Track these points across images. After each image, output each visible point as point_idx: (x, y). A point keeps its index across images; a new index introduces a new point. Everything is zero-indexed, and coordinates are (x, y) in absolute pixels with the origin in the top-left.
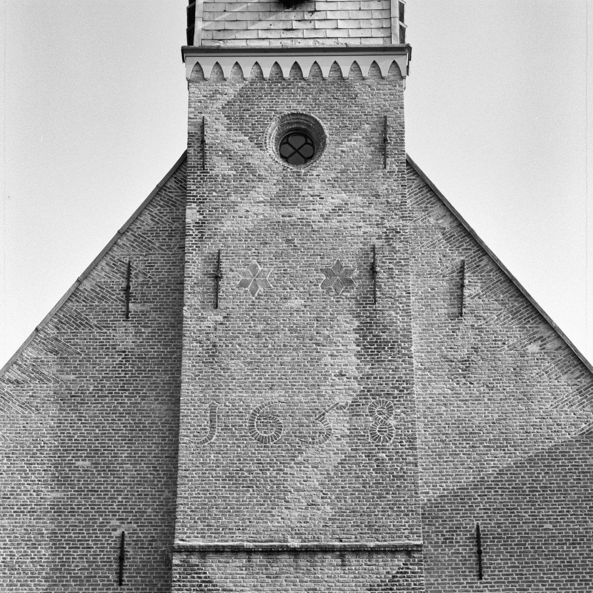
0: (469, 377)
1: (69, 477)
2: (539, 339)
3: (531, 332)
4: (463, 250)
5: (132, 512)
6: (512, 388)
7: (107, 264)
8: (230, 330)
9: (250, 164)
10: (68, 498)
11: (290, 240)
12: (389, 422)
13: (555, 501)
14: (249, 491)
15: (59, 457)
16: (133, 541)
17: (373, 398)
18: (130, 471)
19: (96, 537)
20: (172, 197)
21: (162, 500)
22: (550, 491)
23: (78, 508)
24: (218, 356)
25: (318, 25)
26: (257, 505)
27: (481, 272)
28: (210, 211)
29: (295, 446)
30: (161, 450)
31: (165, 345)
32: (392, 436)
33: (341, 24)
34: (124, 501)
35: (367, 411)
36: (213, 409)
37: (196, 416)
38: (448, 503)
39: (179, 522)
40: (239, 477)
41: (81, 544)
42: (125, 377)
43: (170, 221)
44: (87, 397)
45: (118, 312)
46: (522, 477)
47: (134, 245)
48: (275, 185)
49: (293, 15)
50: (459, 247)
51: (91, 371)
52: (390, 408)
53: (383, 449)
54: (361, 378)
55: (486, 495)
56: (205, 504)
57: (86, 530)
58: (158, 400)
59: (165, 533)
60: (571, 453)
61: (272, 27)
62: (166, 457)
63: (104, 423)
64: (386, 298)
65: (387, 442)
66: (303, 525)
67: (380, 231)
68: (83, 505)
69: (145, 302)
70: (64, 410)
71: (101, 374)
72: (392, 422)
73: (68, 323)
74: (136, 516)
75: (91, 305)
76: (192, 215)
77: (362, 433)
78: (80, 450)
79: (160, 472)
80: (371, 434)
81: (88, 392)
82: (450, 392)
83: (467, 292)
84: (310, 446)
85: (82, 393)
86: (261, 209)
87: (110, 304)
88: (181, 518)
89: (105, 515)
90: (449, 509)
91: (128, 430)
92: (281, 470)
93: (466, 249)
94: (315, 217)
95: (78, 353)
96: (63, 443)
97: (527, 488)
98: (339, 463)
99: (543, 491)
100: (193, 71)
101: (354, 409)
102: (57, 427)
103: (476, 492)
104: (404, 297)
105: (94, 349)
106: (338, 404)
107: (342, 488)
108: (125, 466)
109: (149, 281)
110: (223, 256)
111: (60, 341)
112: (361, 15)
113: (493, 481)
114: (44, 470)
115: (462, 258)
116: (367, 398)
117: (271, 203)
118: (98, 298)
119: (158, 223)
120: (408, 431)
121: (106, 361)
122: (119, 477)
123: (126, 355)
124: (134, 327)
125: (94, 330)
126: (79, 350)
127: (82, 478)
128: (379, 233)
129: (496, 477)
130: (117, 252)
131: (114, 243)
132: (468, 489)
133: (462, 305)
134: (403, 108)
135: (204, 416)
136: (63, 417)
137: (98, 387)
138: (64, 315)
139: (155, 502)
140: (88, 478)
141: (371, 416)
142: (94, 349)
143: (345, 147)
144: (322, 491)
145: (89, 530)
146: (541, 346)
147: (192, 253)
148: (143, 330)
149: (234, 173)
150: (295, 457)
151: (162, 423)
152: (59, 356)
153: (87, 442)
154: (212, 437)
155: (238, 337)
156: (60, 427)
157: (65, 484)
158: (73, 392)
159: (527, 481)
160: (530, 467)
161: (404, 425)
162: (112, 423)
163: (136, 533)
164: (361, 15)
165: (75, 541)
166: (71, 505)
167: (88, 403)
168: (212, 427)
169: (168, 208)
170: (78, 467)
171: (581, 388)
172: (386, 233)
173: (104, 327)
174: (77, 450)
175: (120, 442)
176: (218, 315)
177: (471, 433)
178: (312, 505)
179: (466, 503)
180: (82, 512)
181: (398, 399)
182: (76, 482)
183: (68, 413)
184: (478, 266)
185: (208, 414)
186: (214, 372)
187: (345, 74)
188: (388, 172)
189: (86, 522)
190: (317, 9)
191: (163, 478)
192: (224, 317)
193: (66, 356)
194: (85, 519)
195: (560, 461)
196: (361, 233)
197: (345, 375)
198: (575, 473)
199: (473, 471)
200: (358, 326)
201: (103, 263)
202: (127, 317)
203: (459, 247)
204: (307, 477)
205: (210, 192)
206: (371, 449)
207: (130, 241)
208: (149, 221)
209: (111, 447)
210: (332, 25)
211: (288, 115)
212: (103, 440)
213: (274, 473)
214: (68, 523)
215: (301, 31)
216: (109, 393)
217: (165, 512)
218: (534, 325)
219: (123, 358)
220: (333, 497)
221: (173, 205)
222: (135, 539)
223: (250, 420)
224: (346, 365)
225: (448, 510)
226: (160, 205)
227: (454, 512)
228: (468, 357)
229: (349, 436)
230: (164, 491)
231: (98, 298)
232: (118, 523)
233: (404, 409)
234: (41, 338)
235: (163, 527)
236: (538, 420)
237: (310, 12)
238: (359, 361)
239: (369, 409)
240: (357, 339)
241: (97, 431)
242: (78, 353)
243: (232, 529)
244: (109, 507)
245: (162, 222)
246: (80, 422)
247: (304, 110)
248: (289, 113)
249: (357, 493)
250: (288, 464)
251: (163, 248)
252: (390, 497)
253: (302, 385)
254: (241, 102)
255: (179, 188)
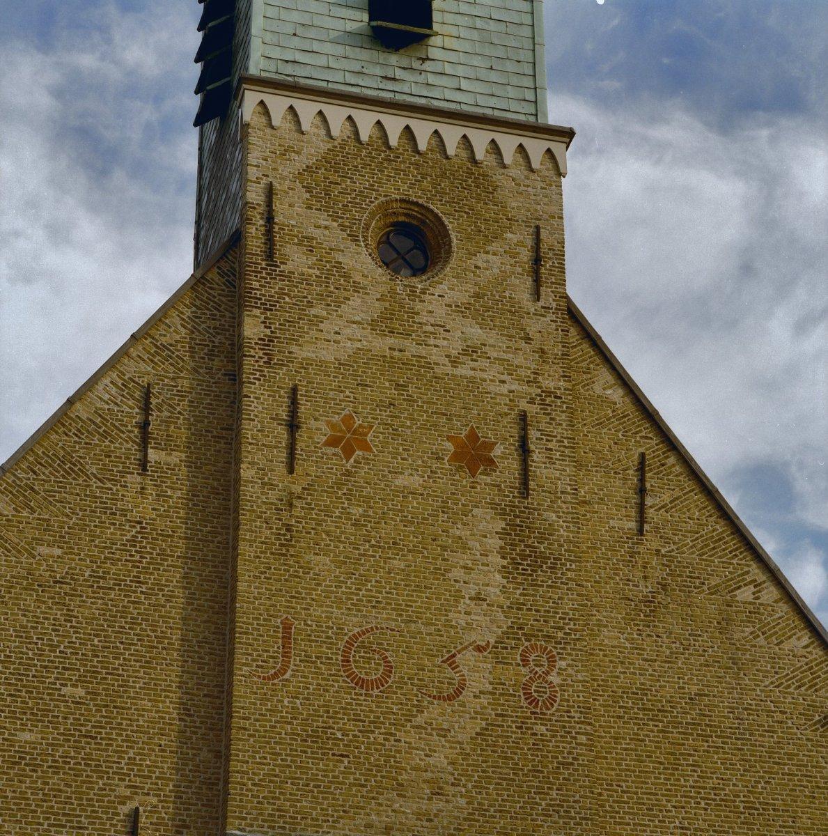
0: (654, 626)
1: (49, 711)
2: (751, 583)
3: (740, 572)
4: (642, 437)
5: (150, 777)
6: (716, 649)
7: (112, 382)
8: (313, 509)
9: (340, 263)
10: (47, 744)
11: (402, 386)
12: (550, 678)
13: (780, 826)
14: (342, 762)
15: (34, 676)
16: (151, 823)
17: (526, 640)
18: (148, 711)
19: (93, 811)
20: (214, 297)
21: (198, 762)
22: (774, 810)
23: (65, 763)
24: (294, 547)
25: (432, 79)
26: (354, 785)
27: (668, 475)
28: (280, 324)
29: (412, 700)
30: (198, 684)
31: (204, 521)
32: (555, 701)
33: (464, 84)
34: (138, 758)
35: (519, 658)
36: (287, 627)
37: (261, 636)
38: (629, 813)
39: (235, 800)
40: (328, 739)
41: (67, 821)
42: (140, 562)
43: (211, 331)
44: (81, 585)
45: (129, 459)
46: (734, 785)
47: (156, 360)
48: (377, 300)
49: (394, 59)
50: (636, 433)
51: (86, 545)
52: (552, 661)
53: (542, 718)
54: (509, 607)
55: (683, 807)
56: (275, 776)
57: (76, 799)
58: (193, 604)
59: (202, 817)
60: (801, 757)
61: (365, 70)
62: (205, 696)
63: (107, 631)
64: (543, 491)
65: (548, 709)
66: (425, 823)
67: (535, 391)
68: (72, 758)
69: (172, 450)
70: (44, 602)
71: (103, 553)
72: (555, 678)
73: (50, 466)
74: (157, 784)
75: (86, 443)
76: (252, 328)
77: (511, 692)
78: (68, 669)
79: (195, 718)
80: (524, 694)
81: (82, 578)
82: (628, 645)
83: (649, 501)
84: (435, 702)
85: (72, 579)
86: (357, 331)
87: (117, 445)
88: (236, 794)
89: (108, 779)
90: (631, 822)
91: (145, 646)
92: (391, 734)
93: (646, 438)
94: (436, 356)
95: (67, 516)
96: (41, 655)
97: (741, 802)
98: (477, 734)
99: (763, 809)
100: (254, 112)
101: (496, 651)
102: (32, 627)
103: (668, 801)
104: (569, 494)
105: (92, 511)
106: (475, 642)
107: (483, 772)
108: (139, 702)
109: (178, 418)
110: (301, 395)
111: (38, 493)
112: (493, 76)
113: (693, 787)
114: (11, 695)
115: (641, 450)
116: (519, 639)
117: (374, 325)
118: (99, 433)
119: (193, 332)
120: (578, 696)
121: (112, 534)
122: (130, 720)
123: (142, 528)
124: (155, 485)
125: (91, 483)
126: (68, 511)
127: (72, 714)
128: (531, 394)
129: (697, 781)
130: (130, 367)
131: (123, 352)
132: (657, 794)
133: (642, 520)
134: (562, 218)
135: (273, 636)
136: (41, 613)
137: (98, 572)
138: (43, 452)
139: (187, 765)
140: (81, 715)
141: (524, 666)
142: (92, 511)
143: (482, 262)
144: (453, 774)
145: (81, 799)
146: (754, 594)
147: (255, 384)
148: (169, 493)
149: (318, 273)
150: (412, 716)
151: (198, 642)
152: (36, 515)
153: (80, 657)
154: (286, 671)
155: (325, 521)
156: (37, 628)
157: (43, 722)
158: (58, 576)
159: (740, 792)
160: (744, 771)
161: (573, 686)
162: (121, 633)
163: (155, 812)
164: (493, 76)
165: (58, 814)
166: (52, 755)
167: (81, 596)
168: (286, 655)
169: (208, 312)
170: (64, 696)
171: (811, 661)
172: (540, 396)
173: (109, 480)
174: (64, 668)
175: (132, 663)
176: (294, 483)
177: (659, 710)
178: (439, 794)
179: (654, 816)
180: (70, 769)
181: (562, 646)
182: (60, 720)
183: (50, 608)
184: (663, 465)
185: (281, 635)
186: (289, 571)
187: (480, 156)
188: (543, 307)
189: (77, 786)
190: (430, 57)
191: (200, 728)
192: (303, 489)
193: (47, 517)
194: (76, 781)
195: (786, 767)
196: (505, 391)
197: (485, 600)
198: (807, 787)
199: (664, 769)
200: (503, 529)
201: (107, 381)
202: (145, 469)
203: (636, 433)
204: (430, 750)
205: (282, 294)
206: (524, 718)
207: (149, 353)
208: (179, 326)
209: (118, 669)
210: (452, 83)
211: (396, 200)
212: (105, 657)
213: (381, 739)
214: (48, 784)
215: (408, 84)
216: (115, 584)
217: (202, 783)
218: (743, 562)
219: (137, 532)
220: (470, 785)
221: (216, 309)
222: (155, 820)
223: (344, 651)
224: (488, 585)
225: (628, 824)
226: (195, 306)
227: (639, 828)
228: (653, 597)
229: (491, 693)
230: (201, 749)
231: (99, 433)
232: (128, 792)
233: (571, 662)
234: (8, 483)
235: (200, 807)
236: (753, 702)
237: (419, 59)
238: (505, 581)
239: (521, 655)
240: (501, 548)
241: (96, 642)
242: (67, 516)
243: (317, 820)
244: (115, 766)
245: (198, 331)
246: (69, 624)
247: (420, 197)
248: (398, 197)
249: (505, 783)
250: (402, 726)
251: (201, 371)
252: (554, 793)
253: (421, 607)
254: (326, 170)
255: (225, 284)
